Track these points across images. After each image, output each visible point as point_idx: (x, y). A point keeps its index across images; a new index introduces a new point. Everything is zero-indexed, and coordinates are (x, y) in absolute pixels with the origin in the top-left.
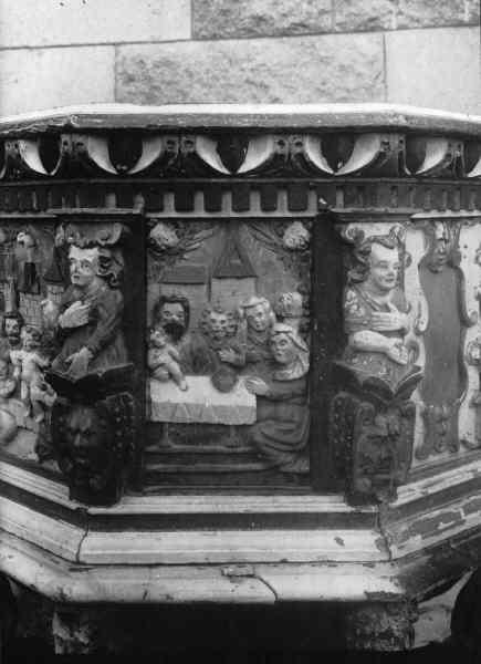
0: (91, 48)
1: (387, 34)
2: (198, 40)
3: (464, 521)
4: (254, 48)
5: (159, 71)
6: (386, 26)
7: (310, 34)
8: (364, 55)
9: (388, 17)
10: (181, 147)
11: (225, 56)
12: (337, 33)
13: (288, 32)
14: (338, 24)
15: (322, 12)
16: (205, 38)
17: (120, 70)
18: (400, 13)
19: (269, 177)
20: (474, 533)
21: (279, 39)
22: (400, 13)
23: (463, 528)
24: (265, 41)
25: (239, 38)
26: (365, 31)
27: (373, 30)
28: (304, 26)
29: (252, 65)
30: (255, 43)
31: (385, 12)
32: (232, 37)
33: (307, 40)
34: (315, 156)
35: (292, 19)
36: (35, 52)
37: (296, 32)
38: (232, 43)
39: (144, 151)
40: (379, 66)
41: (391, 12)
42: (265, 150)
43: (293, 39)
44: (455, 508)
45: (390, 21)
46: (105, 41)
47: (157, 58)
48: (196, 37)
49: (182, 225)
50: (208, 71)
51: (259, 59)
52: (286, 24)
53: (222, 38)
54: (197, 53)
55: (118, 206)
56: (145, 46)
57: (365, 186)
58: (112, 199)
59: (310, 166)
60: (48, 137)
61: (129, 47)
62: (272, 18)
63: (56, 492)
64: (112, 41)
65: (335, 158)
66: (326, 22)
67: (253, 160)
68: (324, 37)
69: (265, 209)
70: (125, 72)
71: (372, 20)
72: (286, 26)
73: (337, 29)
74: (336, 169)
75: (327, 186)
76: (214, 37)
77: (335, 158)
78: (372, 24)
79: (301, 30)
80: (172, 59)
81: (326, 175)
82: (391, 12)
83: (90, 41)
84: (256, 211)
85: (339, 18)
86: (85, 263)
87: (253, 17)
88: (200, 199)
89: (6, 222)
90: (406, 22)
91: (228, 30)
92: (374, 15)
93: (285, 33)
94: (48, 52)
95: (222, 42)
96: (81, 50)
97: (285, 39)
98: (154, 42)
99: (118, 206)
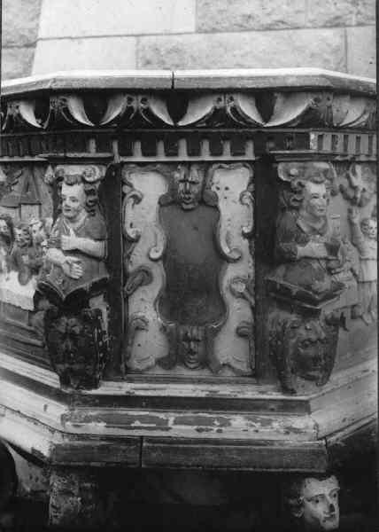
0: (119, 39)
1: (348, 29)
2: (200, 33)
3: (170, 428)
4: (244, 39)
5: (170, 56)
6: (347, 23)
7: (287, 29)
8: (329, 45)
9: (349, 16)
10: (137, 104)
11: (221, 45)
12: (308, 28)
13: (272, 27)
14: (310, 22)
15: (298, 12)
16: (206, 32)
17: (141, 54)
18: (359, 13)
19: (294, 128)
20: (164, 442)
21: (263, 33)
22: (359, 13)
23: (164, 434)
24: (254, 34)
25: (233, 31)
26: (331, 27)
27: (337, 26)
28: (283, 22)
29: (242, 52)
30: (246, 35)
31: (347, 12)
32: (227, 30)
33: (285, 33)
34: (248, 109)
35: (275, 17)
36: (76, 41)
37: (276, 27)
38: (226, 35)
39: (188, 112)
40: (341, 54)
41: (351, 12)
42: (296, 106)
43: (273, 33)
44: (171, 417)
45: (351, 19)
46: (130, 33)
47: (170, 46)
48: (199, 31)
49: (9, 167)
50: (207, 56)
51: (247, 49)
52: (268, 21)
53: (220, 31)
54: (200, 42)
55: (97, 151)
56: (160, 37)
57: (295, 135)
58: (92, 145)
59: (245, 118)
60: (41, 98)
61: (146, 38)
62: (258, 16)
63: (51, 379)
64: (135, 32)
65: (267, 113)
66: (301, 19)
67: (197, 114)
68: (298, 31)
69: (213, 154)
70: (143, 57)
71: (337, 18)
72: (269, 22)
73: (309, 25)
74: (176, 119)
75: (261, 136)
76: (214, 31)
77: (177, 114)
78: (337, 21)
79: (282, 26)
80: (180, 47)
81: (258, 126)
82: (351, 12)
83: (105, 33)
84: (183, 156)
85: (311, 17)
86: (73, 199)
87: (244, 16)
88: (161, 147)
89: (5, 164)
90: (363, 20)
91: (224, 25)
92: (339, 13)
93: (269, 28)
94: (86, 41)
95: (218, 35)
96: (112, 39)
97: (268, 32)
98: (166, 34)
99: (97, 151)
